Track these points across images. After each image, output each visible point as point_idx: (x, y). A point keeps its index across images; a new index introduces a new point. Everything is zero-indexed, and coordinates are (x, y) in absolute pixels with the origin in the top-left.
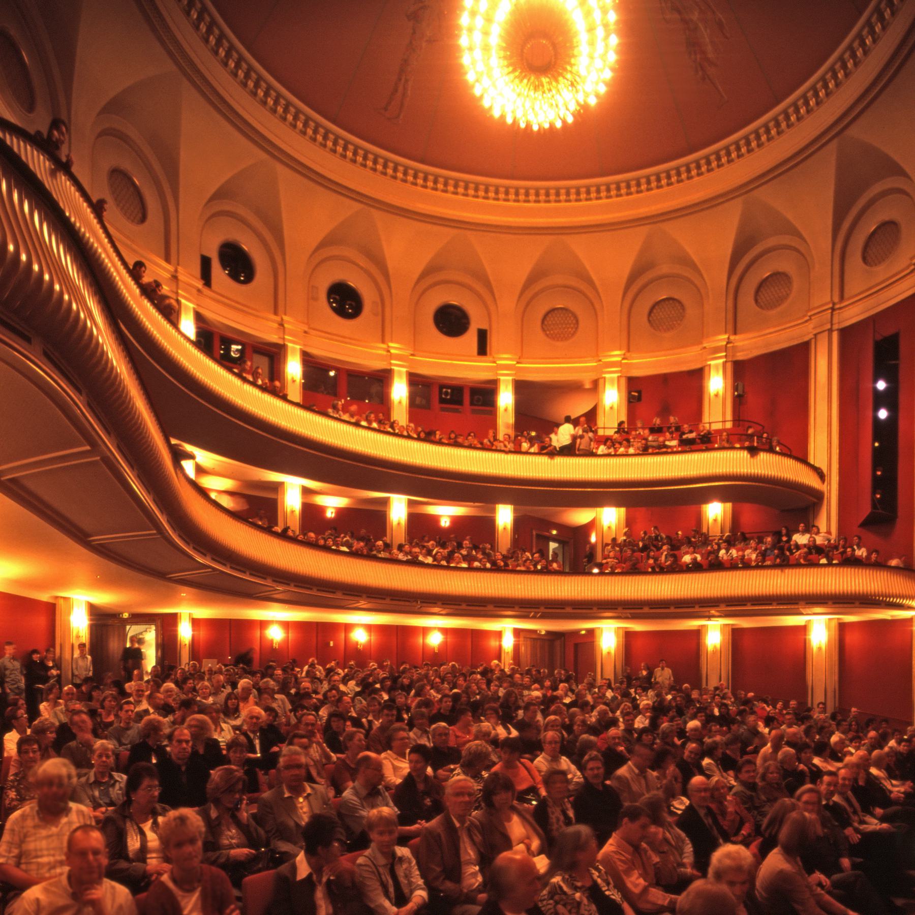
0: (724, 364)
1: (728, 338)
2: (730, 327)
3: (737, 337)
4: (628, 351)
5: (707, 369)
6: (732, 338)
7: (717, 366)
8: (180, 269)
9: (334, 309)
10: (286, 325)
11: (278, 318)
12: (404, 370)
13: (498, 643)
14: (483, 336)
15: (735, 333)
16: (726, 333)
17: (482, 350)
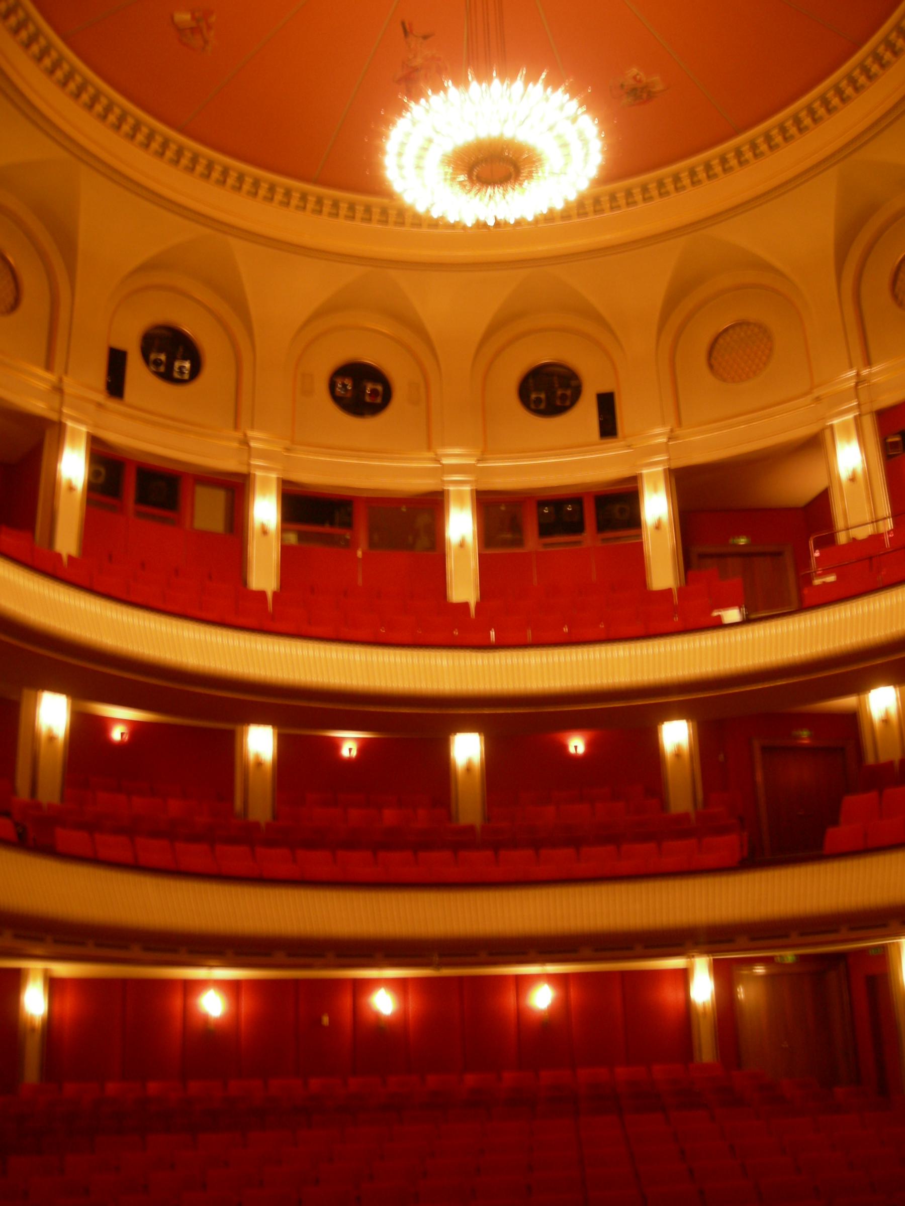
0: (857, 420)
1: (858, 375)
2: (857, 353)
3: (875, 369)
4: (679, 423)
5: (828, 433)
6: (865, 372)
7: (845, 425)
8: (67, 380)
9: (337, 399)
10: (253, 444)
11: (239, 435)
12: (467, 488)
13: (681, 995)
14: (607, 405)
15: (868, 363)
16: (851, 367)
17: (608, 427)
